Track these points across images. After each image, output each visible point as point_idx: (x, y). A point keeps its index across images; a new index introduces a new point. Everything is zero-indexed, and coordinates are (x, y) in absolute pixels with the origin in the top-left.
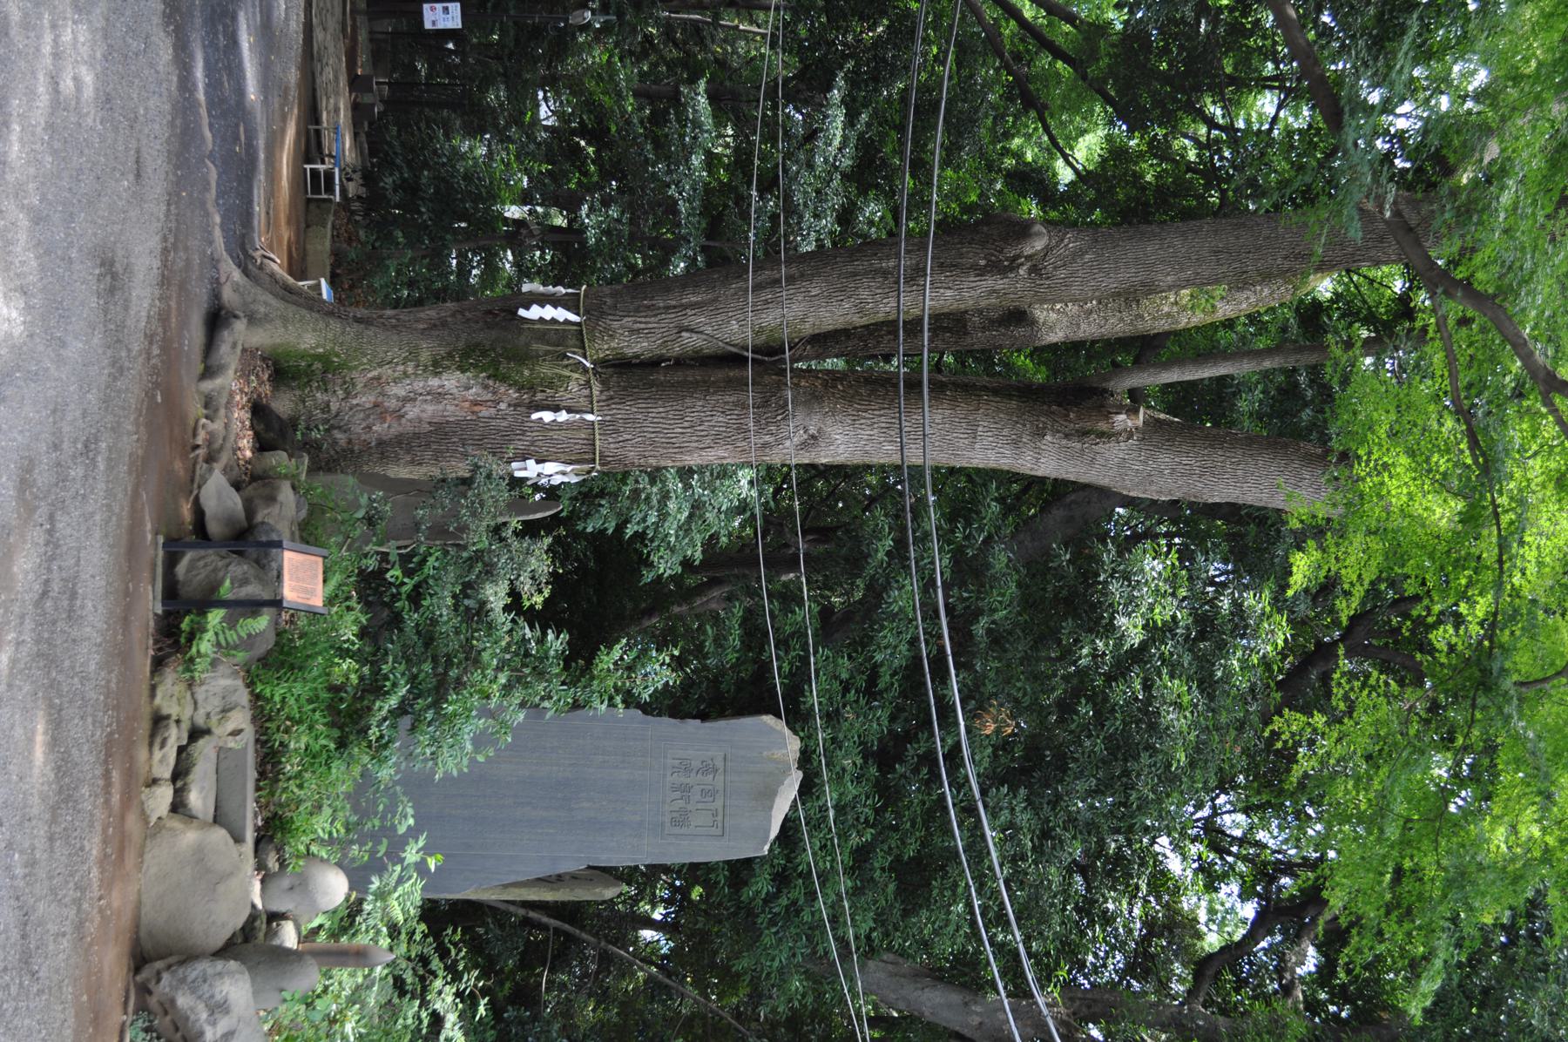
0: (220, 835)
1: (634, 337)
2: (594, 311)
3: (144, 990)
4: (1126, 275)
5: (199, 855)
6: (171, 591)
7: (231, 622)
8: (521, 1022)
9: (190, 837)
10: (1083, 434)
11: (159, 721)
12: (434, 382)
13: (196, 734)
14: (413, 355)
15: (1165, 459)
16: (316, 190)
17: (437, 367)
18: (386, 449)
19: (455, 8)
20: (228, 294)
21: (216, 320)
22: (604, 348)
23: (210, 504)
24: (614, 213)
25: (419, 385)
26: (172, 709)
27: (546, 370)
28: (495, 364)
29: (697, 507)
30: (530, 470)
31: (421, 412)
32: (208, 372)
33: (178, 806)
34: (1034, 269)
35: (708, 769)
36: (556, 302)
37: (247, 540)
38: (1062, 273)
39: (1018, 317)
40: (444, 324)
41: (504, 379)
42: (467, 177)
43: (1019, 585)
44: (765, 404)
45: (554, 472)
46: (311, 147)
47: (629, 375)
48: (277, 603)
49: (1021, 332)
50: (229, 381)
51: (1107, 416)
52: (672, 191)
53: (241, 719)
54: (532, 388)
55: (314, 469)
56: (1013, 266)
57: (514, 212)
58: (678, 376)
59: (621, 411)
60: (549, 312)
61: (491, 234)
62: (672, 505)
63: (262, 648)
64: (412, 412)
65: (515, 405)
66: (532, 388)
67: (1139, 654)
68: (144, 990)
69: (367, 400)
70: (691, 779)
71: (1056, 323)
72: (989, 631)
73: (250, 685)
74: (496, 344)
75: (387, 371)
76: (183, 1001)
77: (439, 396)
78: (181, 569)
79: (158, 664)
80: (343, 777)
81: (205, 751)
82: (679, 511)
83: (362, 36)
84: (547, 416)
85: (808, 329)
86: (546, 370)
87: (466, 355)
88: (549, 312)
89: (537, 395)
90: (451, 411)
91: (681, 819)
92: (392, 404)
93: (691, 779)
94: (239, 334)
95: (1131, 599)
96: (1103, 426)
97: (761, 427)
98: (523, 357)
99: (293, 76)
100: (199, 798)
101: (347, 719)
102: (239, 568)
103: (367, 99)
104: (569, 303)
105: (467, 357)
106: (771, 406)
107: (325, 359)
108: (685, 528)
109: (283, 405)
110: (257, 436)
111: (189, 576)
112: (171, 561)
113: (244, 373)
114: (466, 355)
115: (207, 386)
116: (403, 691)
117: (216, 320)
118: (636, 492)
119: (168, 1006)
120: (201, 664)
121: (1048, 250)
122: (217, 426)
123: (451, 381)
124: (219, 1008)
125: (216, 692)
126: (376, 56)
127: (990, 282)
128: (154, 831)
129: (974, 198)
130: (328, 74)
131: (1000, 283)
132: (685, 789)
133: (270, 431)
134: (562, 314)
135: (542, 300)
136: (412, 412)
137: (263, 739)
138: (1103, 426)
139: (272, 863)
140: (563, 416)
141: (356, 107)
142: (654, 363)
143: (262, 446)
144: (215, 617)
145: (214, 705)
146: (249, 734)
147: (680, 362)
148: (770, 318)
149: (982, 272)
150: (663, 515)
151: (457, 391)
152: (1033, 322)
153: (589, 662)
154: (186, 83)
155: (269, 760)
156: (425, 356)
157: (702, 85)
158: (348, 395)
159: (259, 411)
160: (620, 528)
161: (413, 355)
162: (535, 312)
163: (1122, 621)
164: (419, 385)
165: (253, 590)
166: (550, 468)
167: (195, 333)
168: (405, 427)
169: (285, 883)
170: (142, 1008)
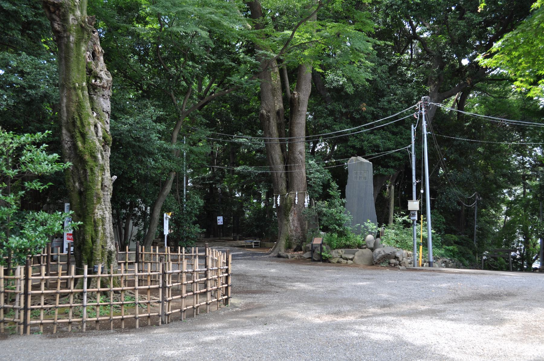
0: (356, 253)
1: (283, 185)
2: (278, 193)
3: (376, 263)
4: (270, 94)
5: (359, 256)
6: (319, 261)
7: (324, 252)
8: (438, 204)
9: (356, 257)
10: (299, 103)
11: (338, 262)
12: (291, 221)
13: (341, 257)
14: (286, 224)
15: (303, 87)
16: (258, 245)
17: (288, 220)
18: (303, 230)
19: (218, 218)
20: (276, 255)
21: (279, 256)
22: (284, 191)
23: (308, 256)
24: (261, 186)
25: (291, 224)
26: (337, 260)
27: (288, 201)
28: (287, 210)
29: (317, 171)
30: (306, 204)
31: (296, 223)
32: (288, 257)
33: (352, 259)
34: (269, 112)
35: (356, 173)
36: (276, 200)
37: (313, 250)
38: (269, 107)
39: (278, 113)
40: (281, 219)
41: (290, 209)
42: (255, 215)
43: (335, 102)
44: (294, 162)
45: (307, 200)
46: (251, 247)
47: (289, 187)
48: (321, 244)
49: (281, 112)
50: (289, 255)
51: (295, 99)
52: (256, 174)
53: (340, 251)
54: (292, 204)
55: (305, 242)
56: (268, 116)
57: (263, 205)
58: (289, 177)
59: (296, 188)
60: (278, 201)
61: (268, 208)
62: (316, 176)
63: (328, 247)
64: (296, 225)
65: (295, 207)
66: (292, 204)
67: (349, 79)
68: (376, 263)
69: (294, 233)
70: (358, 176)
71: (279, 105)
72: (345, 108)
73: (334, 249)
74: (284, 210)
75: (289, 229)
76: (378, 258)
77: (293, 220)
78: (316, 259)
79: (330, 262)
80: (351, 235)
81: (343, 256)
82: (318, 175)
83: (224, 238)
84: (296, 201)
85: (281, 154)
86: (288, 201)
87: (286, 215)
88: (278, 201)
89: (293, 203)
90: (296, 218)
91: (365, 178)
92: (295, 228)
93: (358, 176)
94: (282, 252)
95: (336, 81)
96: (297, 99)
97: (298, 162)
98: (286, 205)
99: (237, 248)
100: (351, 257)
101: (341, 234)
102: (316, 251)
103: (238, 237)
104: (277, 197)
105: (286, 215)
106: (295, 160)
107: (287, 240)
108: (321, 173)
109: (294, 247)
110: (299, 251)
111: (320, 259)
112: (314, 261)
113: (289, 252)
114: (286, 215)
115: (289, 257)
116: (335, 225)
117: (279, 256)
118: (314, 183)
119: (379, 260)
120: (330, 256)
121: (265, 110)
122: (296, 256)
123: (291, 218)
124: (379, 252)
125: (335, 254)
126: (227, 236)
127: (271, 120)
128: (354, 263)
129: (256, 98)
130: (234, 244)
131: (272, 118)
132: (360, 177)
133: (298, 249)
134: (279, 198)
135: (276, 202)
136: (296, 225)
137: (342, 248)
138: (297, 99)
139: (364, 246)
140: (297, 198)
141: (240, 240)
142: (287, 182)
143: (301, 250)
144: (323, 254)
145: (337, 255)
146: (343, 250)
147: (287, 177)
148: (279, 161)
149: (270, 122)
150: (318, 178)
151: (292, 217)
152: (279, 110)
153: (332, 195)
154: (242, 259)
155: (348, 247)
156: (286, 222)
157: (235, 169)
158: (293, 236)
159: (295, 251)
160: (321, 186)
161: (286, 224)
162: (278, 203)
163: (341, 83)
164: (291, 224)
165: (319, 248)
166: (306, 200)
167: (281, 259)
168: (299, 226)
169: (368, 245)
170: (379, 264)
